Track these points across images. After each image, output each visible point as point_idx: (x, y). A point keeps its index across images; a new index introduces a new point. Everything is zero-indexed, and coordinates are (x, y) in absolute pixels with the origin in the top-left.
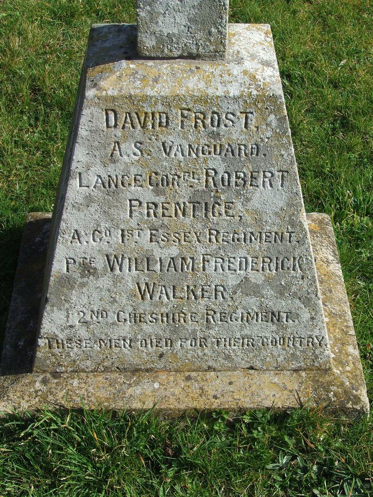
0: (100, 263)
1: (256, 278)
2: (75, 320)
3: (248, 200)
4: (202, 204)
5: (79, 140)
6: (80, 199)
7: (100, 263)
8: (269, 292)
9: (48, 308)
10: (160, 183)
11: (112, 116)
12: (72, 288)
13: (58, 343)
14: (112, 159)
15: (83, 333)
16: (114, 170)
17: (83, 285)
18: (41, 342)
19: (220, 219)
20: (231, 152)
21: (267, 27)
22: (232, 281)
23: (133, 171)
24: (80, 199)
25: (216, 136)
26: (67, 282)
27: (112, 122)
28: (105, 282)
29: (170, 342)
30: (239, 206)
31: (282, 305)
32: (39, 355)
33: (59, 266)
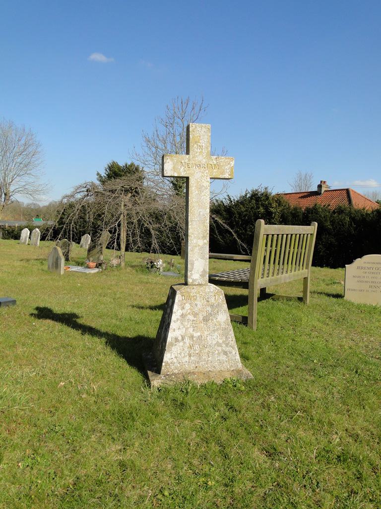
0: (180, 338)
1: (221, 341)
2: (173, 357)
3: (217, 318)
4: (206, 320)
5: (175, 303)
6: (175, 319)
7: (180, 338)
8: (224, 345)
9: (166, 352)
10: (195, 315)
11: (183, 297)
12: (172, 346)
13: (142, 229)
14: (183, 308)
15: (175, 360)
16: (184, 311)
17: (176, 345)
18: (163, 364)
19: (210, 323)
20: (212, 306)
21: (209, 126)
22: (214, 342)
23: (189, 311)
24: (175, 319)
25: (208, 301)
26: (172, 345)
27: (183, 299)
28: (181, 344)
29: (198, 362)
30: (215, 320)
31: (227, 349)
32: (163, 368)
33: (169, 340)
